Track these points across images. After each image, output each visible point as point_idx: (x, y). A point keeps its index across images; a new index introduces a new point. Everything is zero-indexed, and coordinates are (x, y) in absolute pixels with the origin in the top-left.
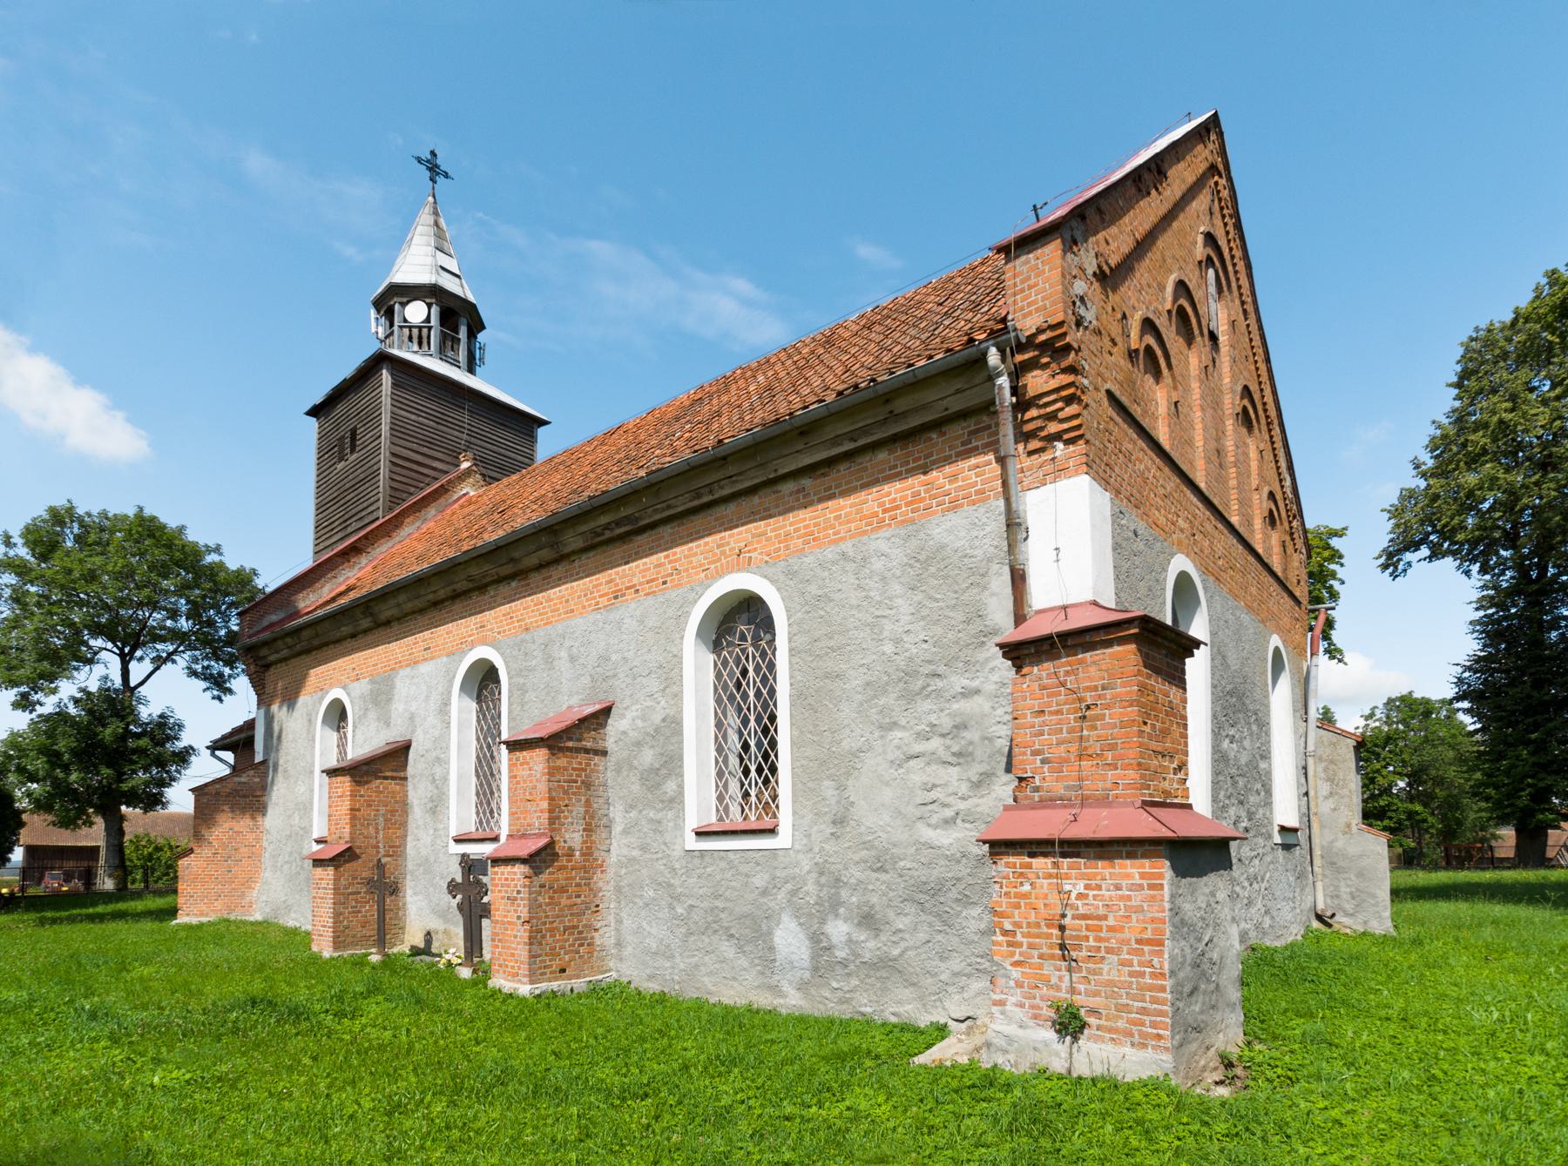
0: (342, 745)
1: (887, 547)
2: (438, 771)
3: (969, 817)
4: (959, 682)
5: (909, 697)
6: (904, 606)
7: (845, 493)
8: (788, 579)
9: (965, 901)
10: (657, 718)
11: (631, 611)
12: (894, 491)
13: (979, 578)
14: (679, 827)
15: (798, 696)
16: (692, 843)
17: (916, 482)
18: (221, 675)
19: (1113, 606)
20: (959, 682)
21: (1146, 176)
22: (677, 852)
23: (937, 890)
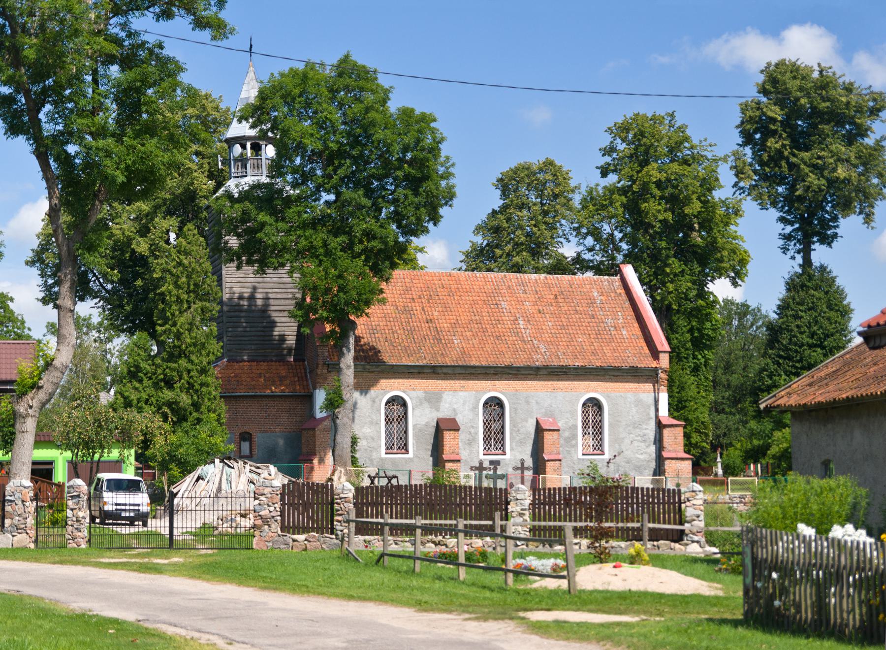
0: (665, 352)
1: (630, 396)
2: (472, 431)
3: (646, 453)
4: (645, 427)
5: (634, 428)
6: (634, 410)
7: (621, 382)
8: (608, 398)
9: (645, 469)
10: (570, 425)
11: (560, 395)
12: (632, 385)
13: (649, 407)
14: (576, 451)
15: (610, 425)
16: (580, 456)
17: (636, 385)
18: (778, 203)
19: (167, 518)
20: (645, 427)
21: (125, 486)
22: (575, 458)
23: (639, 467)
